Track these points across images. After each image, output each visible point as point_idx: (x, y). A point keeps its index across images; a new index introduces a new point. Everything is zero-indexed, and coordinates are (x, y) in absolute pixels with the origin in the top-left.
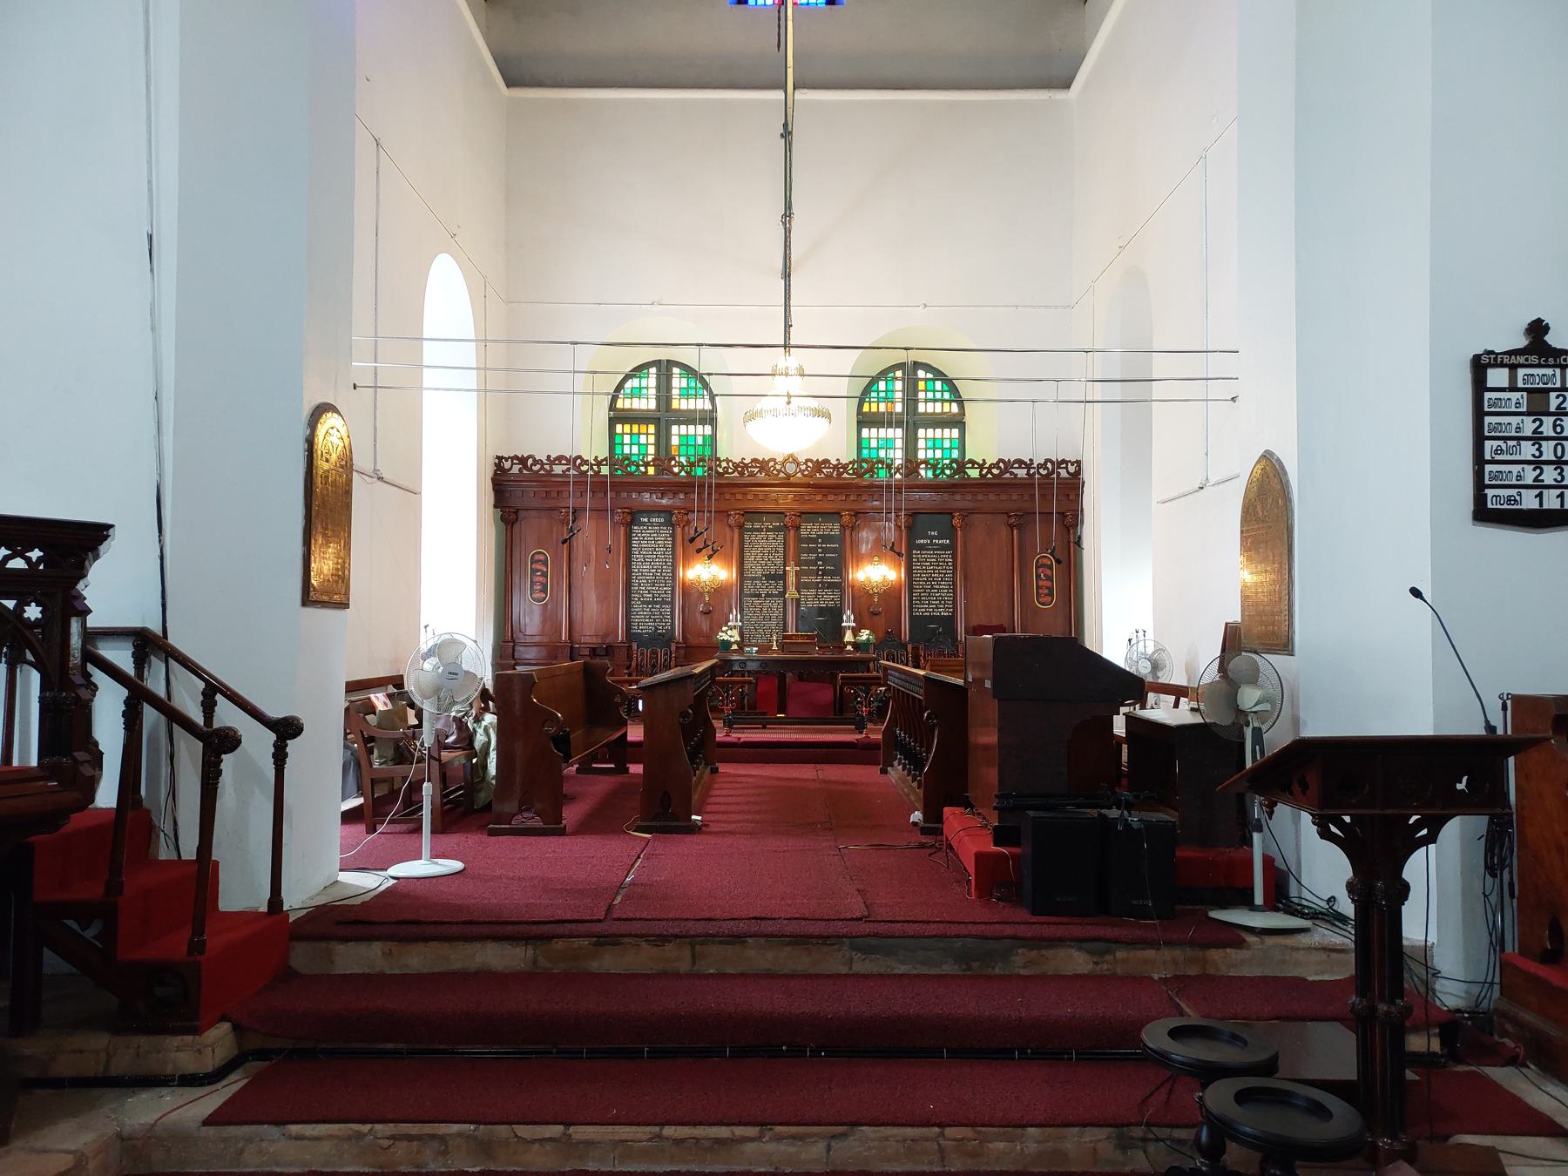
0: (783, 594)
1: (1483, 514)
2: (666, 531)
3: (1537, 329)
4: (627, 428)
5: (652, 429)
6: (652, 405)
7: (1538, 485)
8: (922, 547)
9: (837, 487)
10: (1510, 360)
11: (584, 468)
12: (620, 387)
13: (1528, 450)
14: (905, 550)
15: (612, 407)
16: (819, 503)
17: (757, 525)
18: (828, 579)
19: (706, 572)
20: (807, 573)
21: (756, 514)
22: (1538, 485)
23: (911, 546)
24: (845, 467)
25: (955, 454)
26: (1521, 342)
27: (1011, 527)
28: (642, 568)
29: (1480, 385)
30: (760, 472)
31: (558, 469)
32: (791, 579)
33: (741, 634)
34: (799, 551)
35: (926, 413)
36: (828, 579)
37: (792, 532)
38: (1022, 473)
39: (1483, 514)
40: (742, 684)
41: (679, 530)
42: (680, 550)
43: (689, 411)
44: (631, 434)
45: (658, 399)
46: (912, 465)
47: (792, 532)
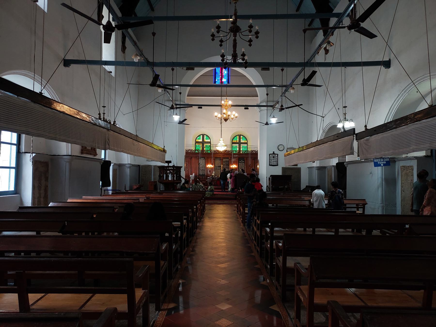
0: (220, 169)
1: (270, 165)
2: (204, 160)
3: (274, 152)
4: (198, 144)
5: (201, 144)
6: (201, 141)
7: (274, 163)
8: (240, 162)
9: (229, 154)
10: (272, 154)
11: (193, 151)
12: (197, 138)
13: (273, 161)
14: (237, 163)
15: (196, 141)
16: (226, 156)
17: (217, 159)
18: (227, 167)
19: (210, 166)
20: (224, 166)
21: (217, 158)
22: (274, 163)
23: (239, 162)
24: (229, 151)
25: (246, 150)
26: (273, 153)
27: (253, 160)
28: (201, 166)
29: (270, 156)
30: (218, 152)
31: (189, 151)
32: (222, 167)
33: (215, 175)
34: (223, 163)
35: (242, 142)
36: (227, 167)
37: (222, 160)
38: (254, 152)
39: (270, 165)
40: (215, 180)
41: (206, 160)
42: (206, 163)
43: (207, 142)
44: (198, 145)
45: (202, 140)
46: (240, 150)
47: (222, 160)
